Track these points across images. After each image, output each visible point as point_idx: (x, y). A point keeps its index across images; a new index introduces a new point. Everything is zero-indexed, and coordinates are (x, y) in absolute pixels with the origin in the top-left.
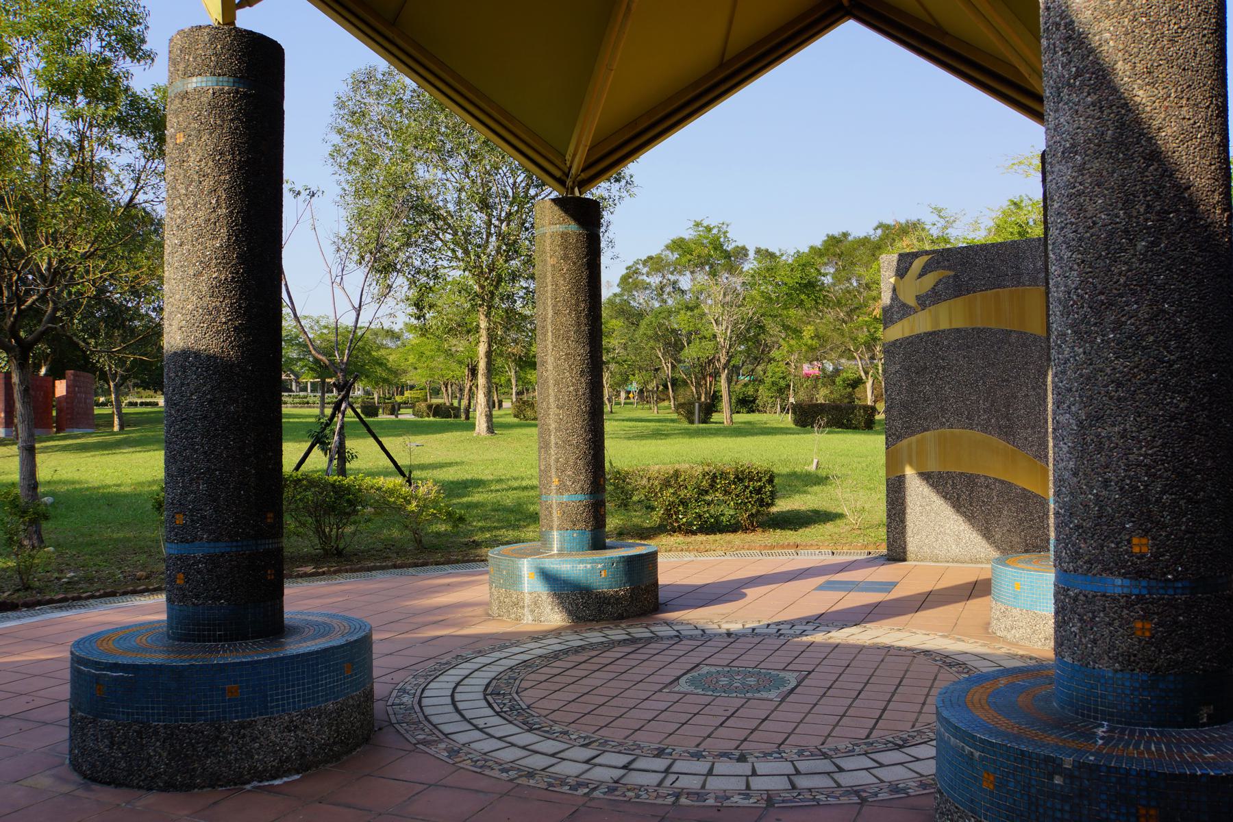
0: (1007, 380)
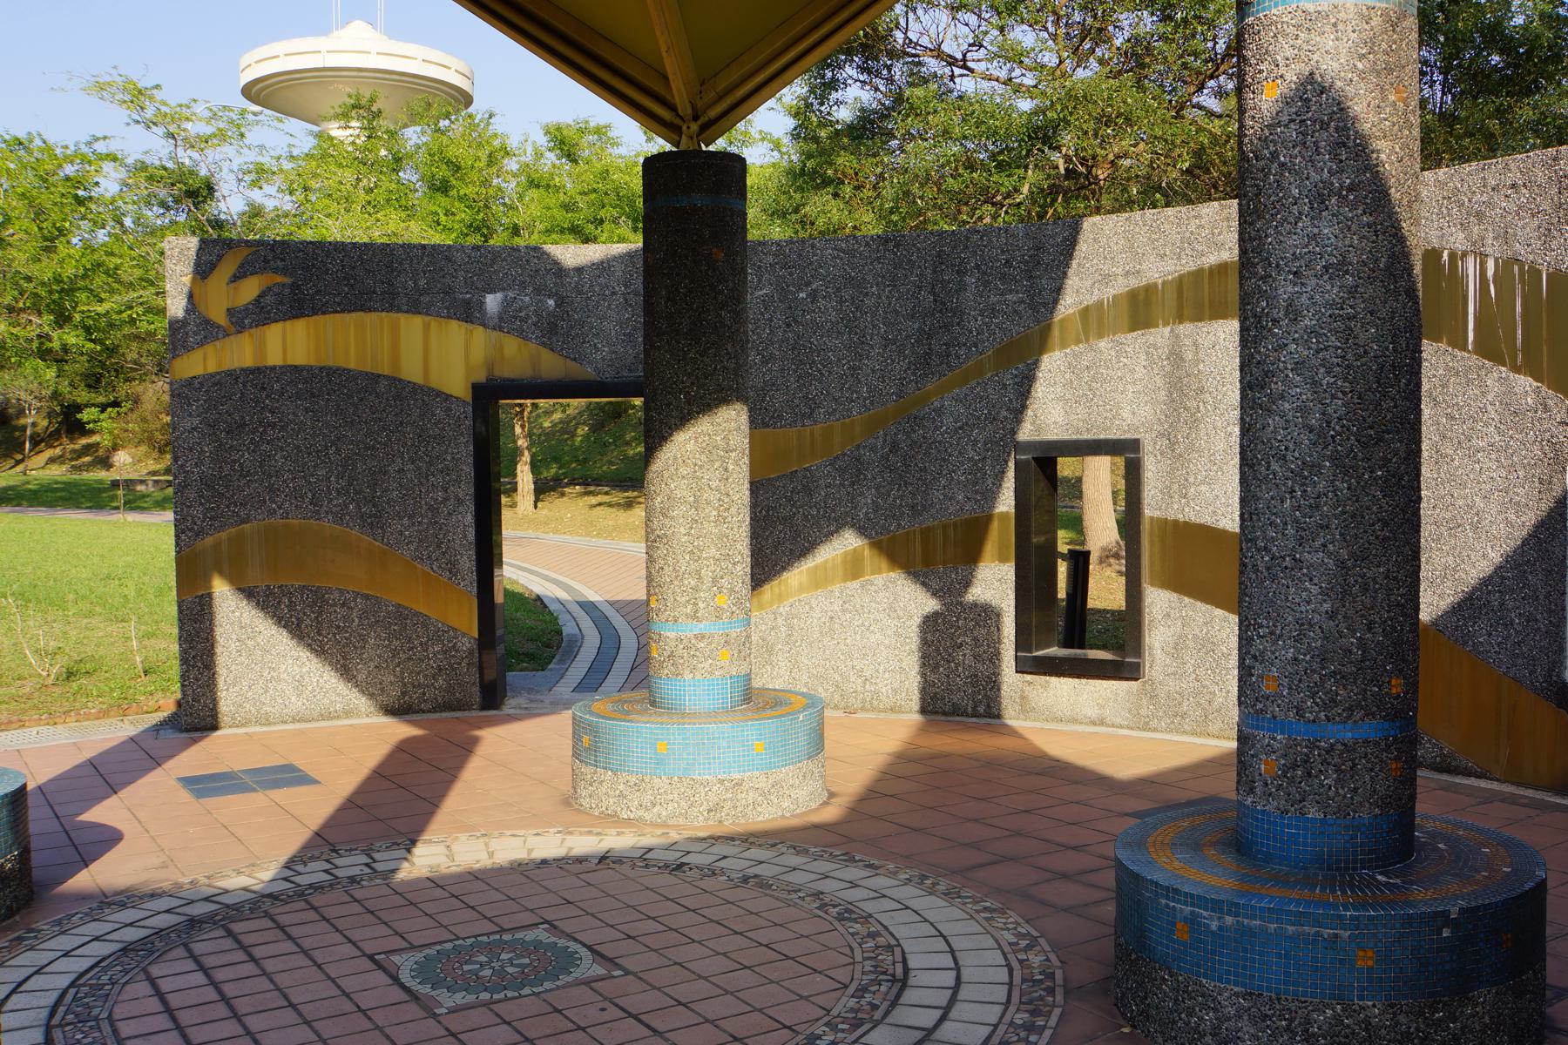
0: (373, 448)
